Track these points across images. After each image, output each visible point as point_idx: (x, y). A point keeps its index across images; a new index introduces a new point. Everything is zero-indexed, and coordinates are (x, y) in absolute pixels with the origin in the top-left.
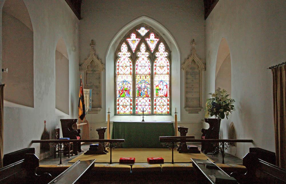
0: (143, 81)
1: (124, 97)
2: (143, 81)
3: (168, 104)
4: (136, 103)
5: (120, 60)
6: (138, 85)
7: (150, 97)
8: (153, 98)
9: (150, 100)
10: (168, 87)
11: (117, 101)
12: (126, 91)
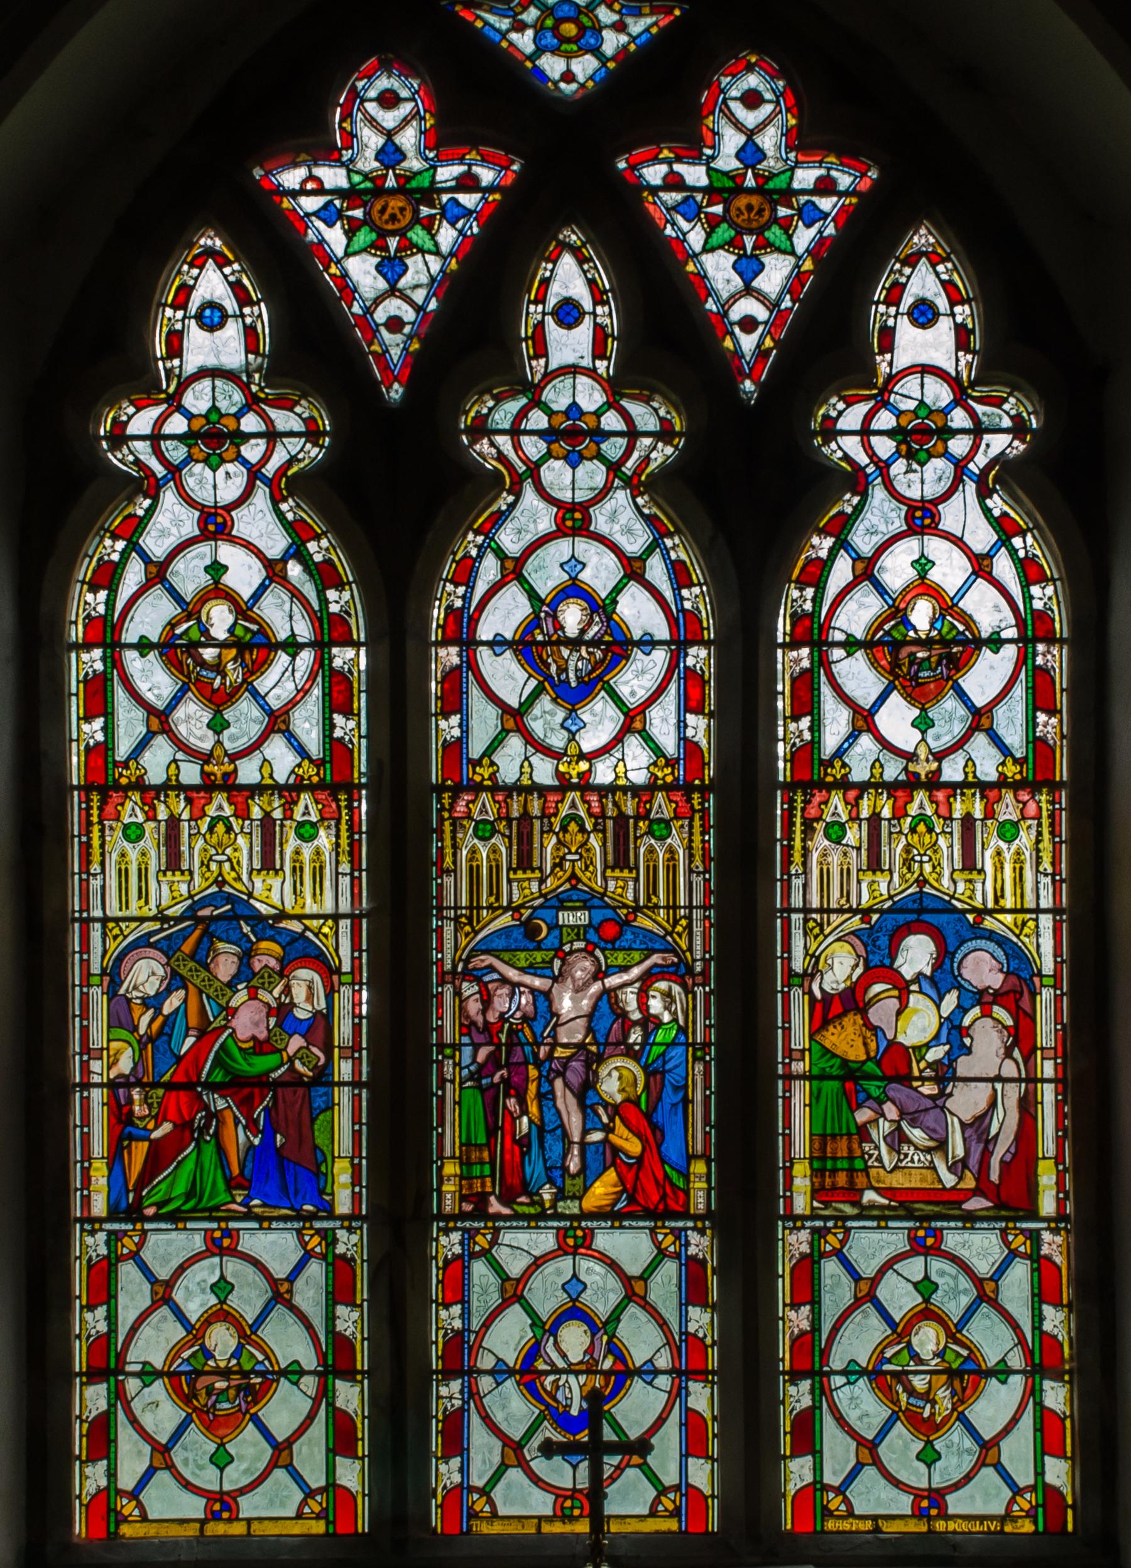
0: (581, 918)
1: (210, 1213)
2: (581, 918)
3: (1048, 1341)
4: (437, 1337)
5: (133, 529)
6: (469, 989)
7: (699, 1202)
8: (771, 1241)
9: (693, 1270)
10: (1046, 1032)
11: (79, 1286)
12: (246, 1106)
